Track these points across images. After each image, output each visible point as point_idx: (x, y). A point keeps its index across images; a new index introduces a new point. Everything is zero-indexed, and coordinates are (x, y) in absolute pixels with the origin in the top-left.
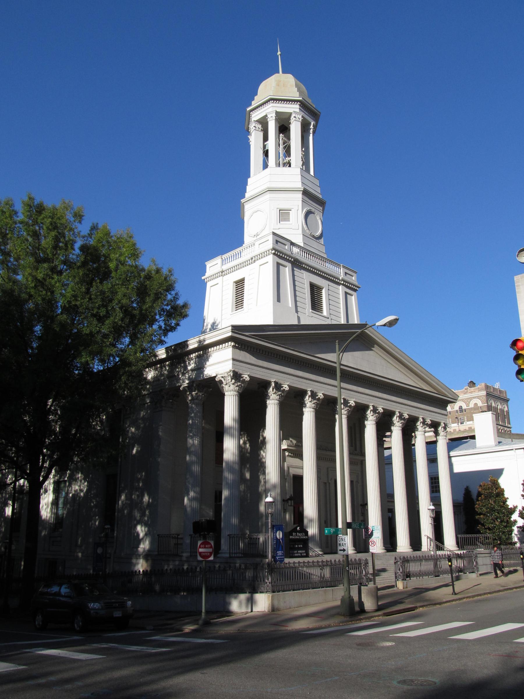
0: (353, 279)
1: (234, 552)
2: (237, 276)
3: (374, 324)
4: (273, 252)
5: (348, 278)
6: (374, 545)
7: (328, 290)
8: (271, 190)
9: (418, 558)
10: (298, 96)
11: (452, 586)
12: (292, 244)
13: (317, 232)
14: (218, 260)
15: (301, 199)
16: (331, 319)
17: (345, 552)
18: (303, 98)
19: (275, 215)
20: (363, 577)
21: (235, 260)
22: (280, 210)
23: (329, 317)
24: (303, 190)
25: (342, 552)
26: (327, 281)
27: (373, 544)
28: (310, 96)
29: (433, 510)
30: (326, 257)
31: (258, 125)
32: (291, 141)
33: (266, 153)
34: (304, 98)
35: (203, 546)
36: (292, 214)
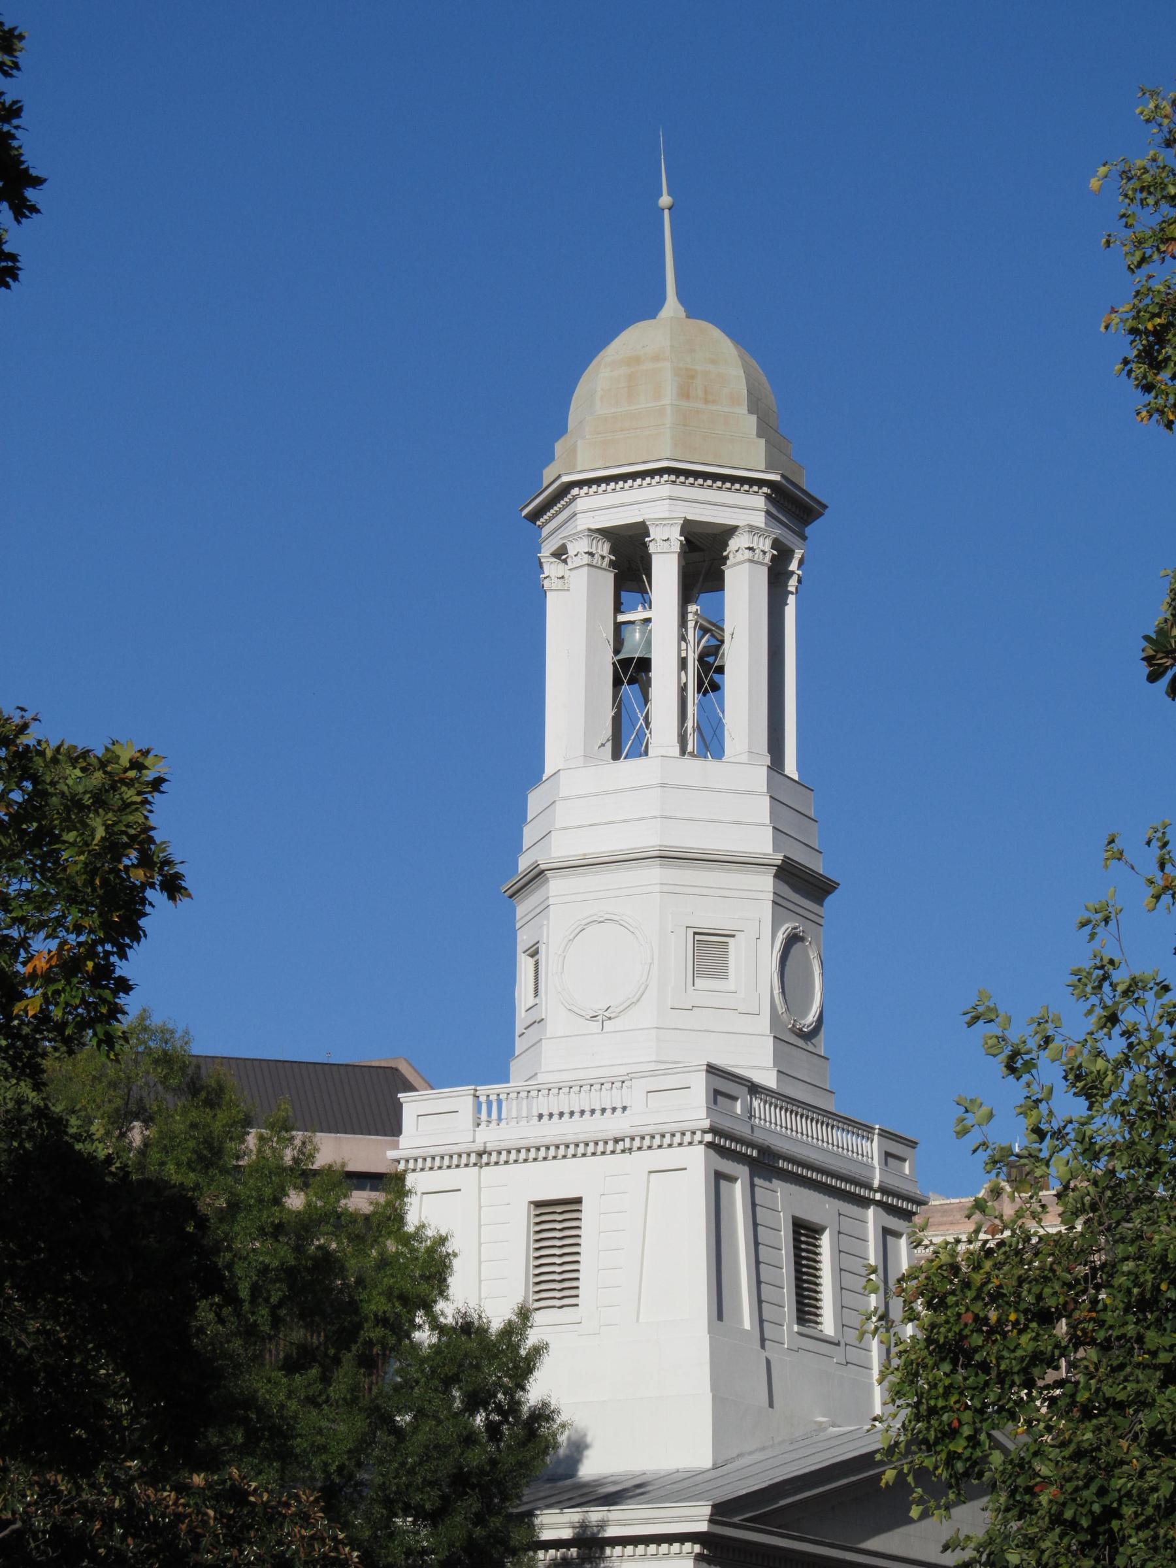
4: (709, 1138)
7: (839, 1233)
8: (668, 857)
10: (763, 467)
12: (754, 1089)
13: (805, 1014)
14: (460, 1099)
15: (771, 896)
16: (846, 1344)
18: (783, 476)
19: (680, 949)
22: (695, 933)
23: (841, 1340)
24: (779, 862)
26: (836, 1201)
31: (600, 544)
34: (786, 474)
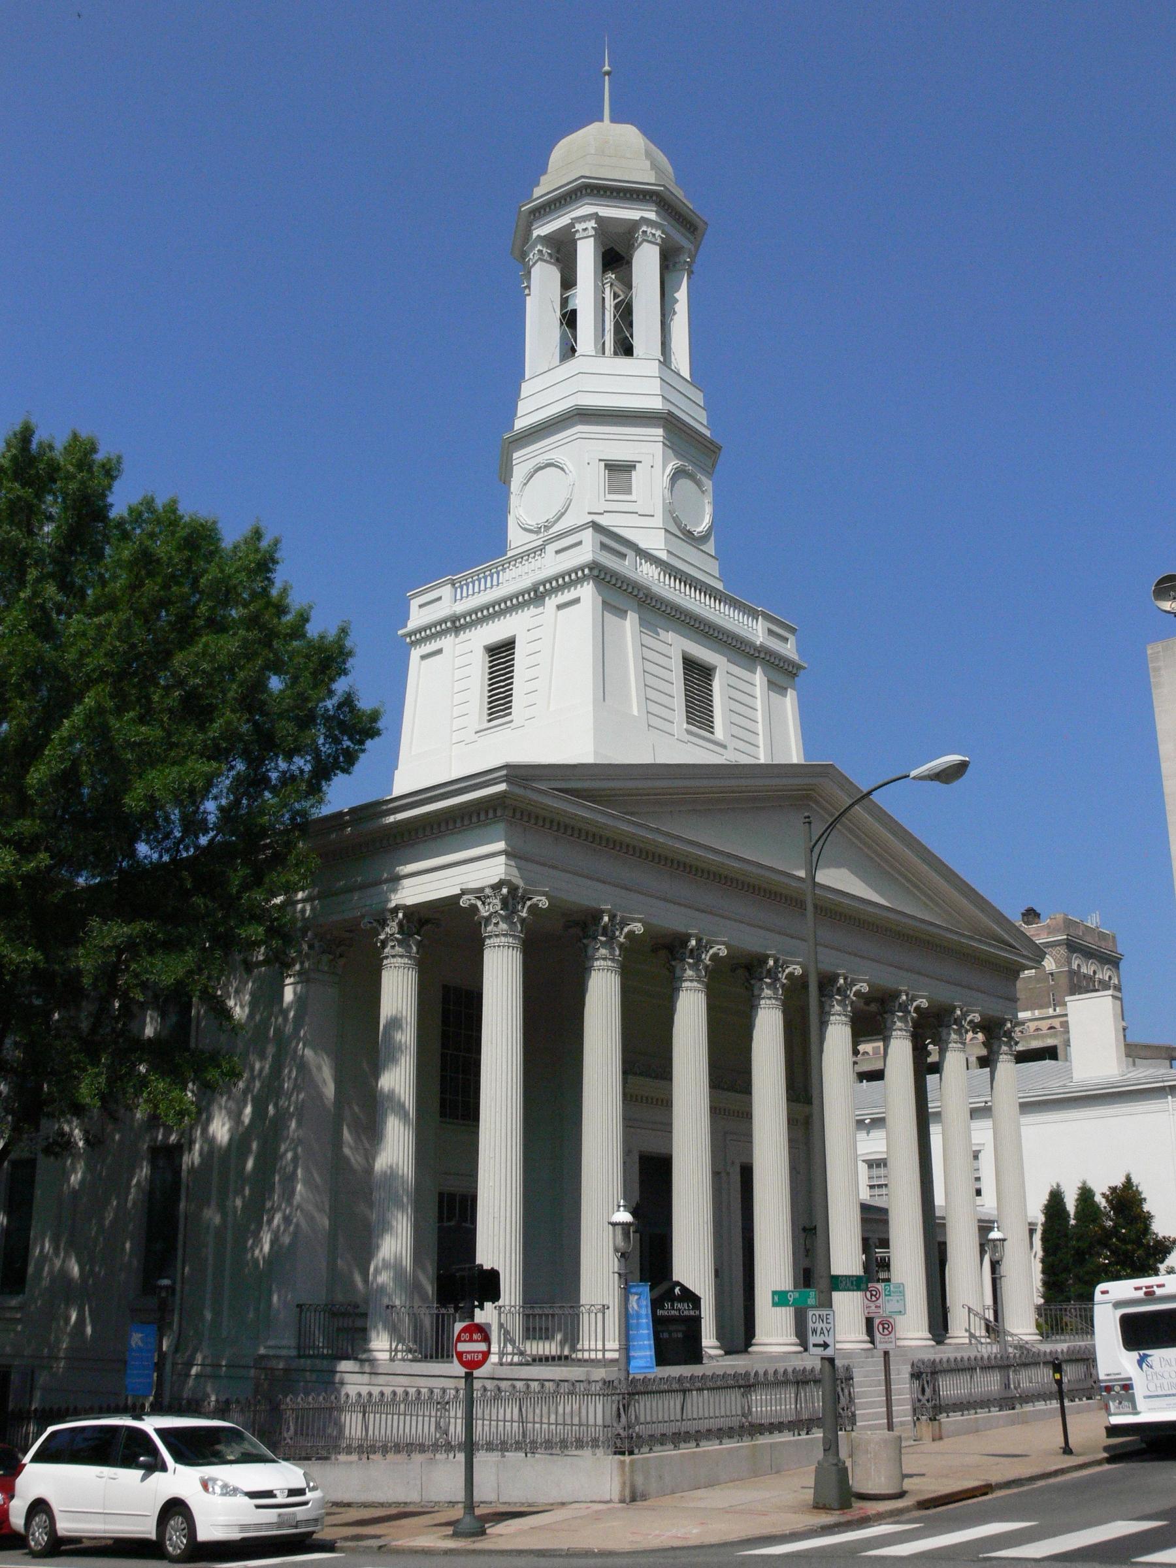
0: (789, 649)
1: (593, 1347)
2: (494, 632)
3: (904, 774)
5: (774, 645)
6: (890, 1333)
9: (966, 1363)
11: (461, 1457)
13: (699, 524)
17: (829, 1349)
20: (841, 1411)
21: (482, 593)
25: (819, 1350)
27: (887, 1329)
28: (679, 182)
29: (625, 1226)
30: (721, 588)
32: (634, 290)
33: (570, 319)
35: (466, 1336)
36: (638, 477)
